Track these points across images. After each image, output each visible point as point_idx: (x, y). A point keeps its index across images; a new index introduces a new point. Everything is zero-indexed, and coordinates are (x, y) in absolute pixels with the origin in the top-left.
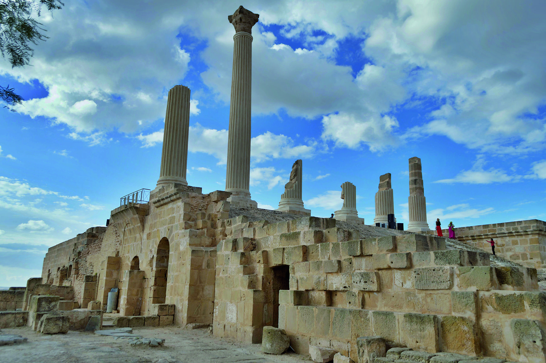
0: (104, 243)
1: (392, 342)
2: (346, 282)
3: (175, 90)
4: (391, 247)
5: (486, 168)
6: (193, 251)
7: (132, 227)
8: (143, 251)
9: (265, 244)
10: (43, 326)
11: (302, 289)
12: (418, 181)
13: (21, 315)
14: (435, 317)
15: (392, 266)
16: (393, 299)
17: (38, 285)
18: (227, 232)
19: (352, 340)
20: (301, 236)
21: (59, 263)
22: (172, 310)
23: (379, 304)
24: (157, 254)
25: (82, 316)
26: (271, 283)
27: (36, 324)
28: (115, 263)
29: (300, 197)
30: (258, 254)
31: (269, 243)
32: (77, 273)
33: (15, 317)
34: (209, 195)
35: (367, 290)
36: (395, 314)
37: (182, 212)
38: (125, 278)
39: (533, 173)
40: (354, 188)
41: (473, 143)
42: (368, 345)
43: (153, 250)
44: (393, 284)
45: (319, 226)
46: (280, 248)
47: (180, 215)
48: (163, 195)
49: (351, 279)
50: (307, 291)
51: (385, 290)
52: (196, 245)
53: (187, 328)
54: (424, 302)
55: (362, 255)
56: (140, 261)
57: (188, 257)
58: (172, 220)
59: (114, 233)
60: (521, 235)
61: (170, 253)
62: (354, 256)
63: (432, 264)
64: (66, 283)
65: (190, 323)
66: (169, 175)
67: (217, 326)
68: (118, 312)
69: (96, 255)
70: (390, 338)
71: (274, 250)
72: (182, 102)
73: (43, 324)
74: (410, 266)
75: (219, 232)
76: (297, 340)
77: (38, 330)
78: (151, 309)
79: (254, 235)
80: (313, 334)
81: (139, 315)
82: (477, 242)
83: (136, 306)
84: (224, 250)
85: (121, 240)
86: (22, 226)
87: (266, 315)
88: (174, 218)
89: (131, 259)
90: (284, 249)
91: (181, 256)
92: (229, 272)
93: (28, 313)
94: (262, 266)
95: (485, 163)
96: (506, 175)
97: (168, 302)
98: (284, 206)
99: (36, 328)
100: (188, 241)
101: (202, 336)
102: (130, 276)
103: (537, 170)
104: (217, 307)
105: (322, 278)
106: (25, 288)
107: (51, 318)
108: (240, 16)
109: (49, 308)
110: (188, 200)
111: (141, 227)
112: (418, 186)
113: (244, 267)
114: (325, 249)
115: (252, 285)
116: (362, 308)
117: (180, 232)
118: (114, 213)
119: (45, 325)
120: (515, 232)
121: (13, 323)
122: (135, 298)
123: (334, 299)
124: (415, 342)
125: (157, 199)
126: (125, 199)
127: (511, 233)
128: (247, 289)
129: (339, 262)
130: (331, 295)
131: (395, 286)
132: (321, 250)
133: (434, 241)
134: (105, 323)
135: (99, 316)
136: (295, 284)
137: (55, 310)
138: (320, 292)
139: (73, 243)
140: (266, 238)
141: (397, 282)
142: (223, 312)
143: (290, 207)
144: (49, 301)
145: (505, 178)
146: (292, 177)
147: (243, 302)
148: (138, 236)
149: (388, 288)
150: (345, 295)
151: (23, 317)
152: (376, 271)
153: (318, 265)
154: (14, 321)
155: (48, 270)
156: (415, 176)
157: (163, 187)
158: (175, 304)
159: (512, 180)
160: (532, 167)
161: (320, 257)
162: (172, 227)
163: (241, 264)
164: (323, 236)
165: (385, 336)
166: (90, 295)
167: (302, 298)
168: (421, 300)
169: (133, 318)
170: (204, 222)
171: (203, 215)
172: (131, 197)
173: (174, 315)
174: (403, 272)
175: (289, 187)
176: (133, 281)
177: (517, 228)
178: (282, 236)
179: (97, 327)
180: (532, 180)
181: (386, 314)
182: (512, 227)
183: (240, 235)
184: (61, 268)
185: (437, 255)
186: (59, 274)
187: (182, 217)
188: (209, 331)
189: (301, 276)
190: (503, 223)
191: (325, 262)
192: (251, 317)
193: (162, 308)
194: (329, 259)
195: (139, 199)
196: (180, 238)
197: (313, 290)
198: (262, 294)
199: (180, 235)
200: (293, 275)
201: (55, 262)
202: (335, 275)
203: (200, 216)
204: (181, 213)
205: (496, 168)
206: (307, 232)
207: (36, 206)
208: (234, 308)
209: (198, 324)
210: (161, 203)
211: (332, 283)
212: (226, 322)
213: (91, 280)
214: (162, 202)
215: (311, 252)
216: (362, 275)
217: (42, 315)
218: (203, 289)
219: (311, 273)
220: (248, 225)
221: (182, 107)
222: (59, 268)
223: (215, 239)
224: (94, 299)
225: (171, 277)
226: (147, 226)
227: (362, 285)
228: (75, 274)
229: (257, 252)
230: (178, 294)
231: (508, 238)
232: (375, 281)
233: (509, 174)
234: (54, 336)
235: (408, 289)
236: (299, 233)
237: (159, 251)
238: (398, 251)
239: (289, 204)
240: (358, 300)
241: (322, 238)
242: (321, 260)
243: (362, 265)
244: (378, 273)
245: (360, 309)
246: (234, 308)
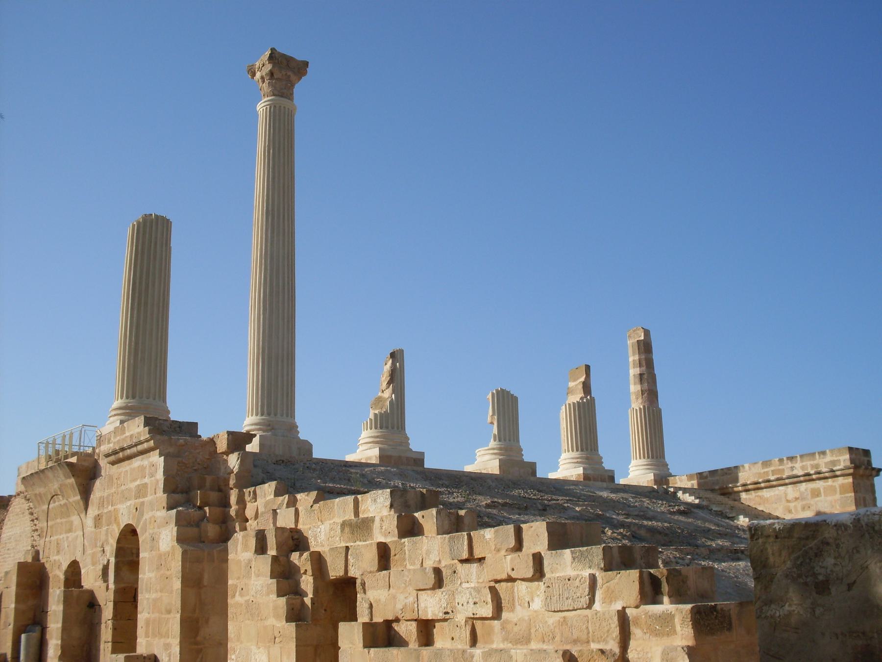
3: (142, 226)
4: (512, 543)
8: (89, 551)
11: (378, 619)
15: (514, 575)
24: (116, 557)
37: (160, 475)
40: (514, 400)
47: (157, 481)
51: (505, 615)
55: (470, 560)
57: (176, 565)
59: (27, 512)
60: (813, 480)
61: (141, 555)
71: (332, 549)
82: (753, 494)
84: (240, 550)
89: (65, 566)
90: (347, 548)
91: (161, 563)
92: (252, 592)
111: (81, 503)
127: (808, 475)
130: (426, 630)
136: (367, 612)
138: (409, 623)
152: (492, 584)
162: (143, 503)
167: (383, 635)
172: (59, 441)
178: (344, 525)
189: (379, 598)
202: (429, 592)
210: (120, 456)
214: (121, 455)
215: (392, 553)
225: (145, 602)
240: (466, 634)
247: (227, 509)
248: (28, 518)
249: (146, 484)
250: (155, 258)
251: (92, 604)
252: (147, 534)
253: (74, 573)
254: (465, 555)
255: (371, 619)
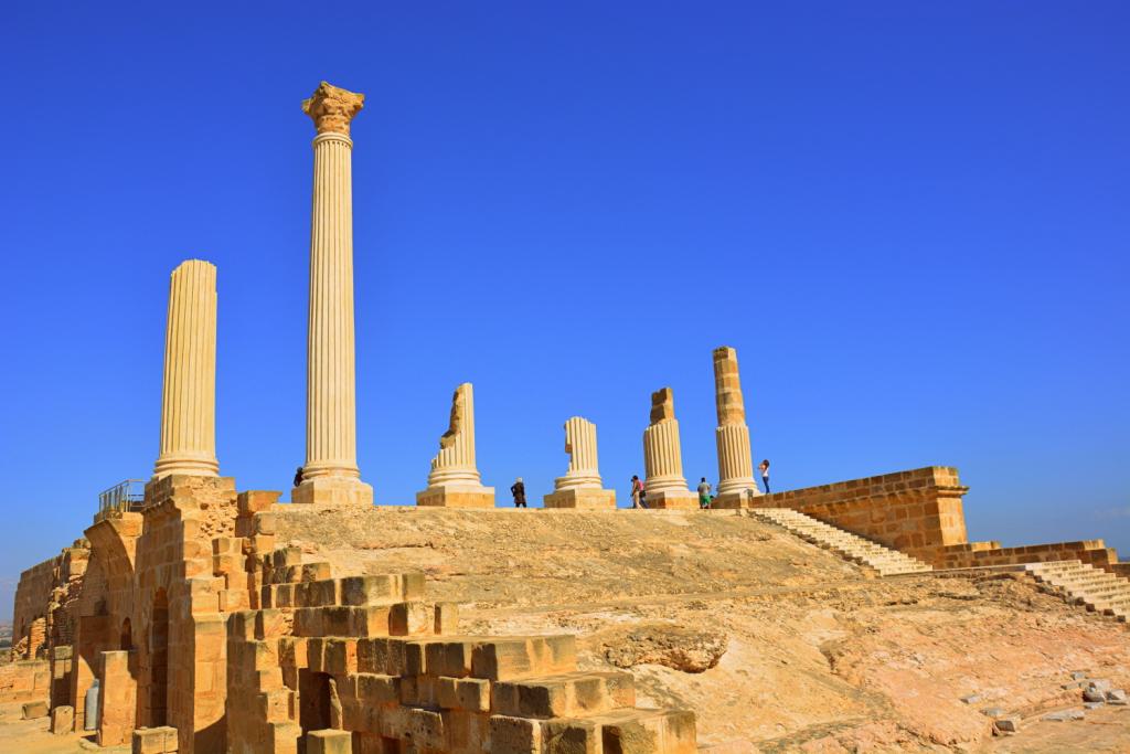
131: (470, 744)
133: (546, 649)
182: (894, 483)
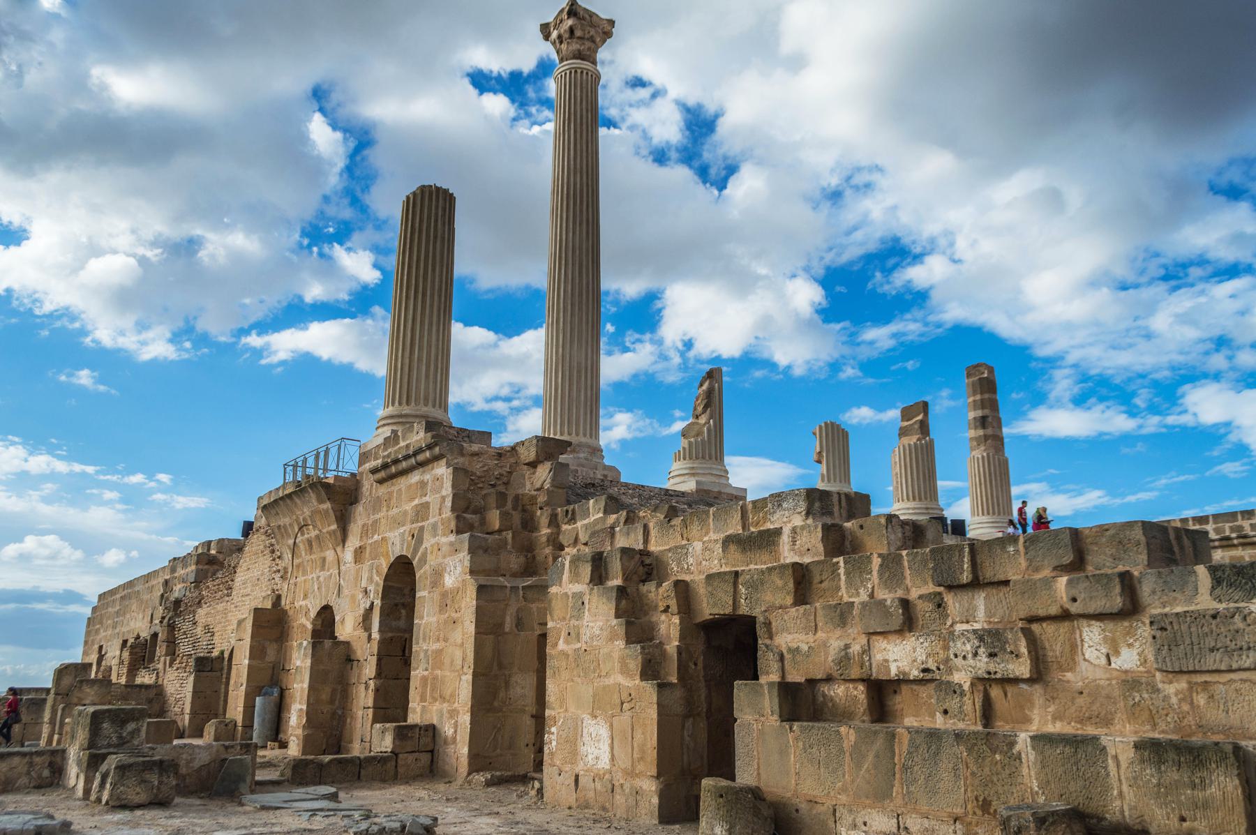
0: (240, 577)
1: (1102, 819)
2: (928, 655)
4: (1068, 558)
5: (1079, 401)
6: (481, 589)
7: (314, 533)
8: (345, 592)
9: (679, 564)
10: (108, 786)
11: (795, 677)
12: (990, 419)
13: (47, 759)
14: (1237, 749)
15: (1074, 608)
16: (1080, 701)
17: (81, 682)
18: (564, 539)
19: (966, 814)
20: (785, 538)
21: (124, 629)
22: (429, 739)
23: (1036, 715)
25: (203, 758)
26: (700, 665)
27: (89, 781)
28: (271, 624)
29: (719, 457)
30: (661, 590)
31: (691, 560)
32: (172, 652)
33: (31, 764)
34: (513, 449)
35: (999, 676)
36: (1104, 741)
37: (447, 490)
38: (300, 660)
39: (1186, 411)
41: (1047, 343)
42: (1038, 829)
43: (371, 588)
44: (1079, 658)
45: (831, 514)
46: (725, 573)
47: (443, 498)
48: (396, 452)
49: (946, 648)
50: (812, 682)
51: (1055, 675)
52: (487, 573)
53: (470, 783)
54: (1186, 707)
55: (976, 583)
56: (337, 618)
57: (469, 602)
58: (422, 512)
59: (267, 551)
62: (950, 588)
63: (1205, 601)
64: (145, 678)
65: (478, 771)
66: (408, 403)
67: (555, 779)
68: (284, 745)
69: (220, 607)
70: (1092, 807)
71: (710, 577)
72: (436, 226)
73: (109, 780)
74: (1131, 609)
75: (544, 539)
76: (794, 814)
77: (93, 797)
78: (371, 737)
79: (646, 541)
80: (843, 798)
81: (338, 752)
83: (329, 727)
84: (569, 585)
85: (285, 569)
86: (12, 549)
87: (695, 748)
88: (426, 506)
89: (313, 614)
90: (736, 573)
92: (584, 638)
93: (64, 751)
94: (676, 620)
95: (1076, 390)
96: (1124, 416)
97: (414, 718)
98: (682, 479)
99: (87, 792)
100: (467, 563)
101: (516, 802)
102: (313, 655)
103: (1195, 404)
104: (554, 729)
105: (856, 648)
106: (48, 691)
107: (131, 765)
108: (570, 22)
109: (120, 737)
110: (460, 460)
112: (989, 431)
113: (628, 624)
114: (859, 568)
115: (650, 670)
116: (985, 726)
117: (444, 540)
118: (265, 502)
119: (114, 785)
120: (1238, 537)
121: (24, 780)
122: (326, 708)
123: (890, 703)
124: (1176, 820)
125: (379, 462)
126: (295, 466)
127: (1228, 538)
128: (638, 682)
129: (905, 604)
130: (882, 694)
131: (1084, 665)
132: (847, 573)
134: (260, 776)
135: (247, 757)
136: (775, 666)
137: (136, 743)
139: (161, 580)
140: (683, 547)
141: (1090, 654)
142: (572, 742)
143: (697, 482)
144: (121, 718)
145: (1120, 423)
146: (700, 409)
147: (627, 716)
148: (330, 555)
149: (1061, 669)
150: (925, 692)
151: (51, 764)
153: (842, 615)
154: (28, 773)
155: (96, 647)
156: (983, 408)
157: (393, 431)
158: (435, 722)
159: (1140, 427)
160: (1183, 396)
161: (843, 591)
162: (422, 529)
163: (617, 616)
164: (843, 537)
165: (1079, 801)
166: (209, 701)
167: (801, 702)
168: (1174, 700)
169: (331, 761)
170: (505, 516)
171: (502, 497)
172: (311, 462)
173: (432, 751)
174: (1110, 625)
175: (693, 433)
176: (322, 667)
177: (1240, 528)
178: (728, 541)
179: (244, 788)
180: (1184, 429)
181: (1075, 742)
182: (1227, 526)
183: (608, 543)
184: (131, 641)
185: (1219, 574)
186: (126, 654)
187: (450, 504)
188: (533, 793)
190: (1207, 517)
191: (864, 605)
192: (652, 755)
193: (403, 733)
194: (872, 596)
195: (332, 466)
196: (444, 557)
197: (829, 679)
198: (678, 693)
199: (444, 549)
200: (768, 642)
201: (114, 627)
203: (492, 501)
204: (444, 493)
205: (1102, 399)
206: (803, 528)
207: (47, 500)
208: (601, 731)
209: (498, 773)
211: (887, 661)
212: (580, 768)
213: (211, 670)
214: (393, 469)
215: (817, 579)
216: (980, 636)
217: (104, 757)
218: (507, 684)
219: (820, 634)
220: (622, 520)
221: (435, 237)
222: (125, 642)
223: (534, 557)
224: (216, 716)
225: (422, 655)
226: (355, 529)
227: (982, 664)
228: (166, 655)
229: (659, 585)
230: (445, 697)
231: (1219, 551)
232: (1024, 650)
233: (1132, 413)
234: (138, 813)
235: (1126, 672)
236: (778, 532)
237: (387, 592)
238: (1090, 568)
239: (693, 475)
240: (972, 704)
241: (843, 544)
242: (846, 599)
243: (980, 610)
244: (1029, 629)
245: (980, 728)
246: (604, 732)
247: (535, 535)
248: (268, 558)
249: (427, 503)
250: (435, 237)
251: (347, 657)
252: (427, 567)
253: (326, 616)
254: (966, 577)
255: (783, 676)
